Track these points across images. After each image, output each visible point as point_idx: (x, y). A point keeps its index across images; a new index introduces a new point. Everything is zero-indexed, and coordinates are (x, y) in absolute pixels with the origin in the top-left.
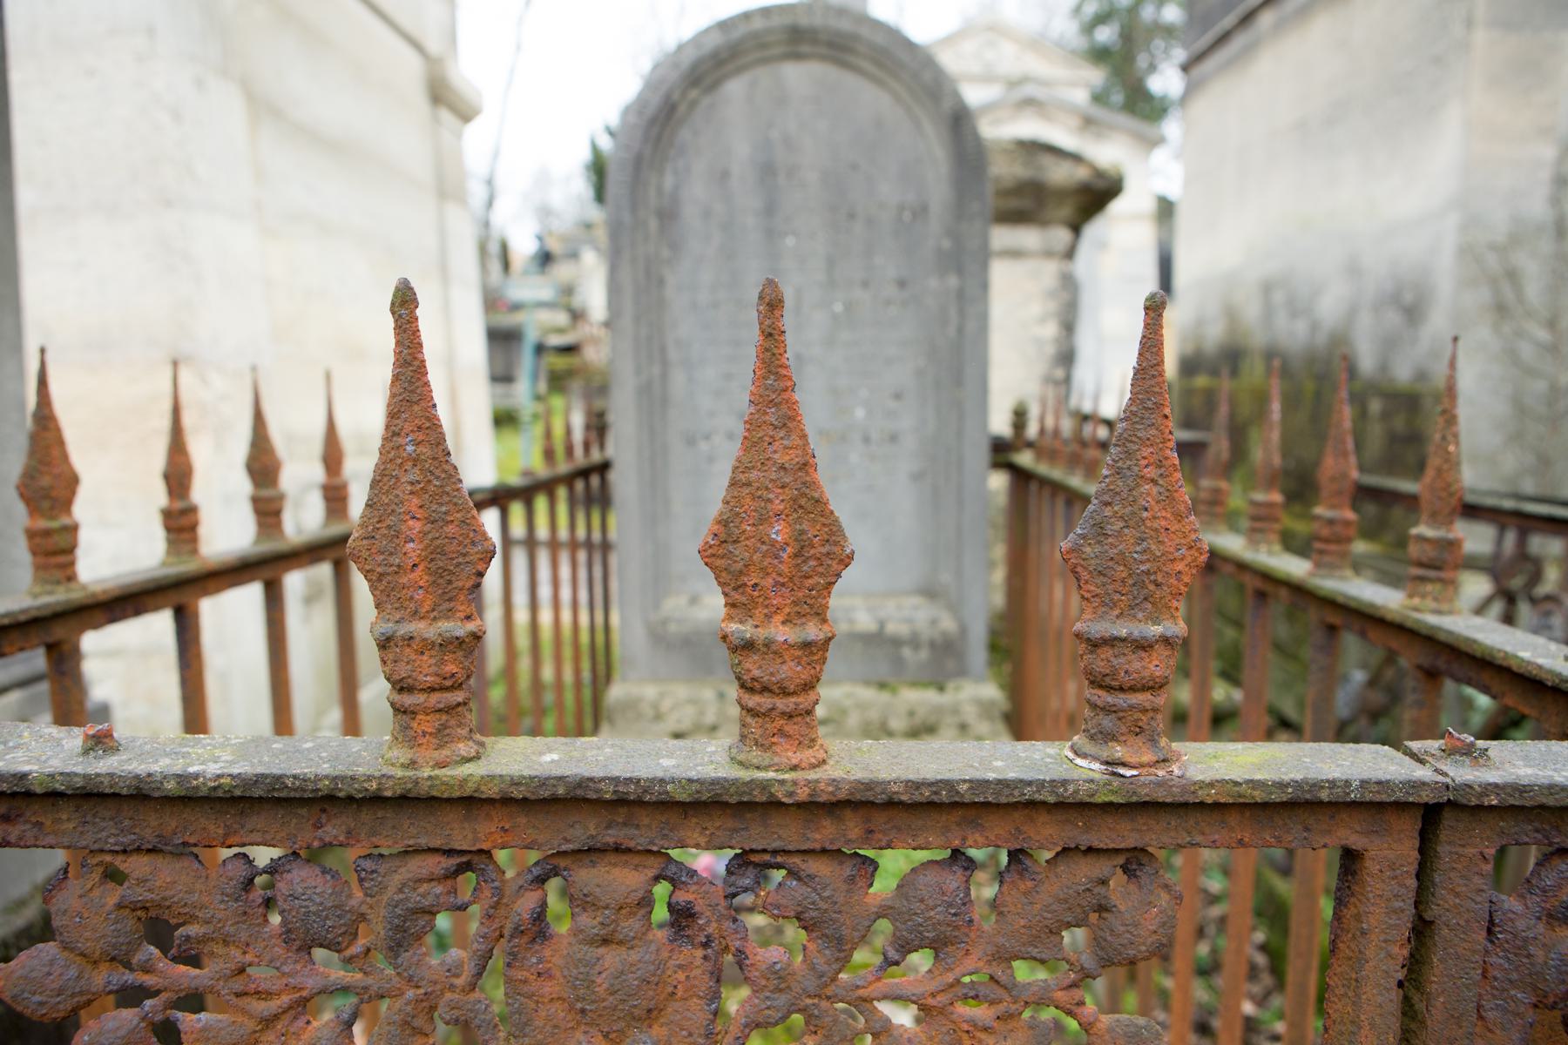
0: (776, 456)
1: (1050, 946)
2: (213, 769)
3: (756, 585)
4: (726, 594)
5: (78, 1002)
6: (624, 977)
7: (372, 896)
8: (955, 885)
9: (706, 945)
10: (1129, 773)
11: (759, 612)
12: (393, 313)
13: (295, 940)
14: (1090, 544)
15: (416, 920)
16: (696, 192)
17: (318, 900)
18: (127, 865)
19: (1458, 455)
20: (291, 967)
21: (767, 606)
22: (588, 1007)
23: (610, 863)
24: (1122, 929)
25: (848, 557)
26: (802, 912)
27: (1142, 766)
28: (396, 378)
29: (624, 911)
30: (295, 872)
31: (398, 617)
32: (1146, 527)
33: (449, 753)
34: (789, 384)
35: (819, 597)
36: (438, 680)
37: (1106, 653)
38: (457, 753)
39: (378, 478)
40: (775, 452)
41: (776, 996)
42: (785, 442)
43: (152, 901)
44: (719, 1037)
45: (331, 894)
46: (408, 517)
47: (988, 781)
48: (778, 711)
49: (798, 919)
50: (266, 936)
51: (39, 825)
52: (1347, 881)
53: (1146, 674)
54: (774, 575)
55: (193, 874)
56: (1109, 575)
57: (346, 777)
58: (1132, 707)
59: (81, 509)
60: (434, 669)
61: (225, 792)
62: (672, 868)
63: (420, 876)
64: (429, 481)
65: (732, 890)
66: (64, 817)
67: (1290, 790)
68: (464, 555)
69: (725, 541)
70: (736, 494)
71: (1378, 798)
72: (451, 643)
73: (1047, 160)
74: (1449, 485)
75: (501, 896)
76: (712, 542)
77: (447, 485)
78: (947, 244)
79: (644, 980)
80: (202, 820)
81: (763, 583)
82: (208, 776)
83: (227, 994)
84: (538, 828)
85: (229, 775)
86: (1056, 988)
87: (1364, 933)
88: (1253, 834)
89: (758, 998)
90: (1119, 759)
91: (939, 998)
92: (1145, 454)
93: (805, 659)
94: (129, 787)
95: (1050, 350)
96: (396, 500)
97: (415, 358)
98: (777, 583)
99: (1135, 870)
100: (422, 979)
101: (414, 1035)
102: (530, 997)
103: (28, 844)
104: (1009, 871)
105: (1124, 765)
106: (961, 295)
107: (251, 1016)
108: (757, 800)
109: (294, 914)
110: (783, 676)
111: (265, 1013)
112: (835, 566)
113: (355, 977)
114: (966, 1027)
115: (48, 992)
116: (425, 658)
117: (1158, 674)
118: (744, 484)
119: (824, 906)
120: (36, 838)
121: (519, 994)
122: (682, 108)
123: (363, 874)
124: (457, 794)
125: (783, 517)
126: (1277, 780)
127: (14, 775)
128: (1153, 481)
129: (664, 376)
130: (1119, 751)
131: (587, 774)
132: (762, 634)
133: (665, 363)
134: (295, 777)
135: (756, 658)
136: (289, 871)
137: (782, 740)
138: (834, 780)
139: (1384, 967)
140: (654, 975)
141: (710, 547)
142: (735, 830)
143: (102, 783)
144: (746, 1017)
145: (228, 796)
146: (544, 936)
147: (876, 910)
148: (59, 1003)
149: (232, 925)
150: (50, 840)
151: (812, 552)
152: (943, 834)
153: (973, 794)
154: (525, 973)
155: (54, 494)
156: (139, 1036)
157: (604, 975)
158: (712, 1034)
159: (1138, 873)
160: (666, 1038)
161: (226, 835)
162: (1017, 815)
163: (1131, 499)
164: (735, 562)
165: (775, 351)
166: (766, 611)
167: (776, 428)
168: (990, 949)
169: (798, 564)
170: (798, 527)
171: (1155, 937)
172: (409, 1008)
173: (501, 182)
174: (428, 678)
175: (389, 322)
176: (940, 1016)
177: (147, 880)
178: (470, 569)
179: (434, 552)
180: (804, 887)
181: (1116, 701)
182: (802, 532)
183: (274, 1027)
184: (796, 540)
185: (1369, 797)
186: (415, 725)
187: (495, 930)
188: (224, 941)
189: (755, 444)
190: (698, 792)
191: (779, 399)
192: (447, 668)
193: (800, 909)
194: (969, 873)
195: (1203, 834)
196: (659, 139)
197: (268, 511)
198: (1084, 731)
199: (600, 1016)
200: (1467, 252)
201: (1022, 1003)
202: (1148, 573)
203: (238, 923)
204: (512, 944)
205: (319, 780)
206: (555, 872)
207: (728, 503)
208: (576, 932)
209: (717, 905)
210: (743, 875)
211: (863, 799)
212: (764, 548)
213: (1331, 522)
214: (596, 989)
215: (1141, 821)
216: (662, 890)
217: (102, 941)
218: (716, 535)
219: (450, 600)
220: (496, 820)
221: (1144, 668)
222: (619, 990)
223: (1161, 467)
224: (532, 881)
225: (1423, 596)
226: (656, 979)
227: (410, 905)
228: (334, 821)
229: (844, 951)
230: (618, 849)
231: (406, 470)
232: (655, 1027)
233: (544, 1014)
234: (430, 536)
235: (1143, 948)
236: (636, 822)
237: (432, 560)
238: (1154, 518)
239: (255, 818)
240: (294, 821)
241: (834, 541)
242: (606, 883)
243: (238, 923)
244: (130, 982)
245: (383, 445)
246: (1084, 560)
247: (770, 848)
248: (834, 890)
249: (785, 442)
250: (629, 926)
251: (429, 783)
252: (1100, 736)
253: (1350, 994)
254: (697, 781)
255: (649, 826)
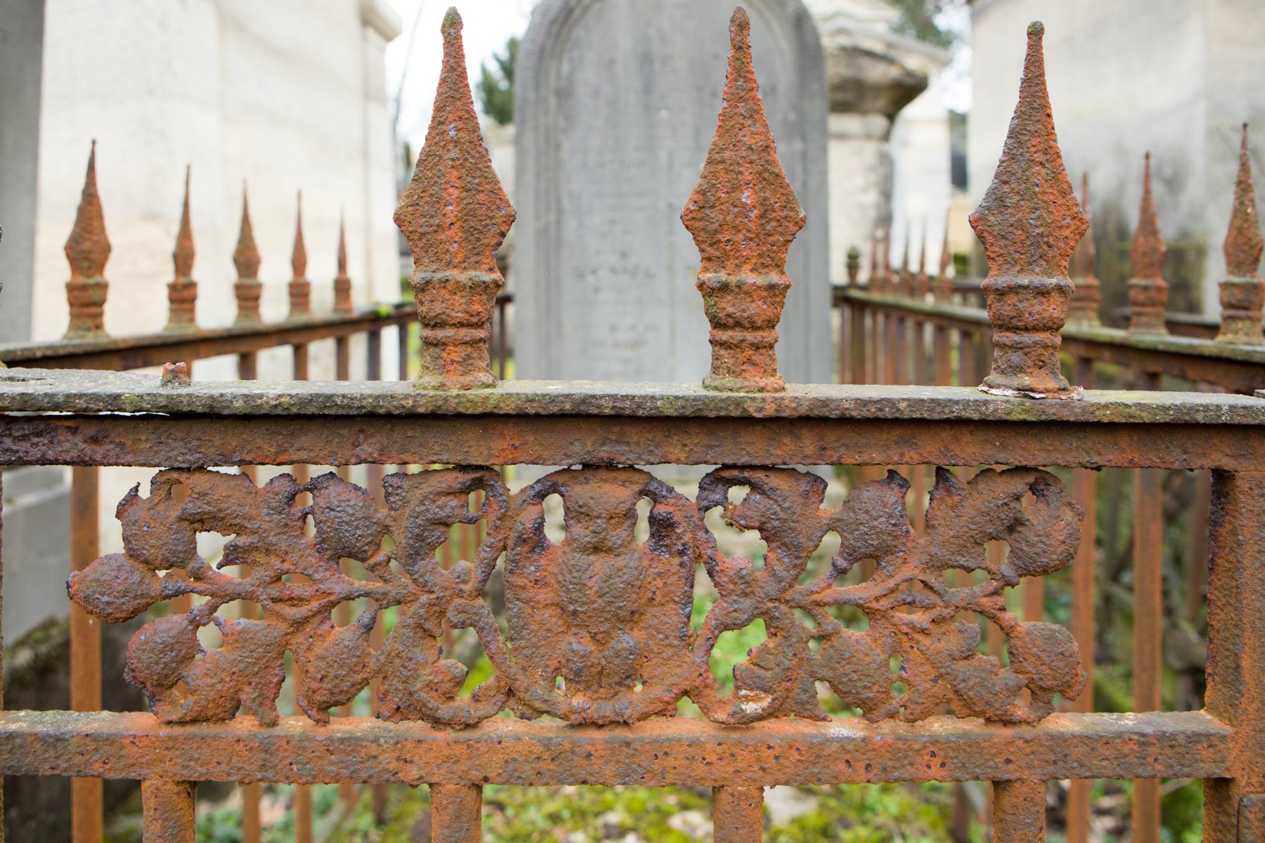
0: (745, 139)
1: (975, 555)
2: (273, 392)
3: (729, 240)
4: (702, 251)
5: (139, 604)
6: (611, 581)
7: (395, 510)
8: (895, 499)
9: (681, 553)
10: (1038, 396)
11: (730, 264)
12: (443, 32)
13: (327, 550)
14: (993, 214)
15: (433, 531)
16: (588, 75)
17: (351, 512)
18: (190, 481)
19: (1256, 215)
20: (322, 574)
21: (737, 258)
22: (579, 609)
23: (602, 480)
24: (1035, 539)
25: (802, 220)
26: (765, 522)
27: (1047, 391)
28: (443, 81)
29: (613, 521)
30: (331, 488)
31: (434, 268)
32: (1039, 199)
33: (472, 378)
34: (754, 85)
35: (779, 252)
36: (467, 316)
37: (1012, 299)
38: (478, 379)
39: (423, 158)
40: (745, 136)
41: (742, 600)
42: (752, 129)
43: (210, 513)
44: (692, 639)
45: (362, 507)
46: (448, 186)
47: (922, 400)
48: (748, 342)
49: (761, 529)
50: (302, 547)
51: (122, 445)
52: (1220, 504)
53: (1046, 315)
54: (744, 231)
55: (246, 490)
56: (1010, 238)
57: (387, 396)
58: (1035, 343)
59: (111, 272)
60: (462, 308)
61: (285, 409)
62: (653, 487)
63: (440, 490)
64: (466, 159)
65: (705, 503)
66: (143, 438)
67: (1171, 412)
68: (491, 218)
69: (703, 207)
70: (712, 170)
71: (1244, 421)
72: (479, 286)
73: (866, 63)
74: (1250, 239)
75: (508, 509)
76: (693, 208)
77: (480, 163)
78: (792, 116)
79: (629, 584)
80: (258, 440)
81: (735, 238)
82: (271, 396)
83: (265, 599)
84: (543, 445)
85: (288, 395)
86: (981, 595)
87: (1239, 544)
88: (1141, 455)
89: (726, 602)
90: (1028, 385)
91: (882, 602)
92: (1034, 143)
93: (770, 299)
94: (203, 406)
95: (872, 214)
96: (439, 174)
97: (459, 66)
98: (746, 239)
99: (1043, 490)
100: (435, 585)
101: (424, 638)
102: (527, 603)
103: (111, 461)
104: (937, 489)
105: (1032, 390)
106: (804, 156)
107: (285, 619)
108: (732, 415)
109: (329, 524)
110: (753, 312)
111: (297, 616)
112: (792, 228)
113: (378, 586)
114: (905, 629)
115: (115, 594)
116: (457, 297)
117: (1056, 315)
118: (719, 162)
119: (782, 515)
120: (118, 456)
121: (518, 599)
122: (577, 12)
123: (390, 490)
124: (479, 410)
125: (751, 185)
126: (1160, 404)
127: (110, 396)
128: (1041, 163)
129: (559, 222)
130: (1027, 380)
131: (591, 392)
132: (733, 280)
133: (560, 211)
134: (344, 396)
135: (729, 298)
136: (326, 488)
137: (750, 368)
138: (796, 398)
139: (1260, 576)
140: (638, 579)
141: (691, 212)
142: (710, 447)
143: (182, 402)
144: (716, 619)
145: (285, 413)
146: (542, 546)
147: (827, 522)
148: (123, 603)
149: (275, 535)
150: (129, 458)
151: (774, 215)
152: (884, 451)
153: (910, 411)
154: (524, 580)
155: (92, 256)
156: (187, 637)
157: (594, 580)
158: (685, 636)
159: (1045, 492)
160: (644, 641)
161: (277, 453)
162: (946, 435)
163: (1025, 178)
164: (712, 223)
165: (744, 60)
166: (737, 262)
167: (745, 118)
168: (924, 558)
169: (763, 224)
170: (762, 194)
171: (1063, 547)
172: (422, 611)
173: (406, 99)
174: (459, 315)
175: (440, 39)
176: (883, 621)
177: (207, 494)
178: (494, 230)
179: (468, 214)
180: (767, 500)
181: (1022, 339)
182: (766, 199)
183: (304, 629)
184: (761, 204)
185: (1237, 420)
186: (444, 355)
187: (500, 540)
188: (267, 549)
189: (727, 131)
190: (683, 407)
191: (747, 96)
192: (474, 307)
193: (763, 519)
194: (904, 490)
195: (1100, 455)
196: (558, 35)
197: (248, 296)
198: (995, 369)
199: (590, 617)
200: (1214, 133)
201: (954, 608)
202: (1042, 235)
203: (279, 534)
204: (515, 552)
205: (364, 398)
206: (554, 489)
207: (705, 177)
208: (569, 542)
209: (692, 516)
210: (714, 491)
211: (821, 415)
212: (736, 210)
213: (1146, 288)
214: (587, 592)
215: (1048, 442)
216: (643, 508)
217: (165, 548)
218: (696, 202)
219: (478, 254)
220: (508, 438)
221: (1045, 310)
222: (606, 593)
223: (1046, 154)
224: (534, 496)
225: (1236, 332)
226: (639, 583)
227: (430, 516)
228: (370, 441)
229: (801, 558)
230: (610, 466)
231: (448, 150)
232: (636, 630)
233: (539, 618)
234: (465, 202)
235: (1055, 557)
236: (627, 440)
237: (466, 221)
238: (1045, 193)
239: (303, 439)
240: (336, 440)
241: (791, 207)
242: (598, 495)
243: (279, 534)
244: (183, 588)
245: (429, 133)
246: (989, 226)
247: (739, 463)
248: (792, 502)
249: (752, 129)
250: (617, 536)
251: (457, 400)
252: (1010, 370)
253: (1231, 601)
254: (682, 398)
255: (638, 444)
